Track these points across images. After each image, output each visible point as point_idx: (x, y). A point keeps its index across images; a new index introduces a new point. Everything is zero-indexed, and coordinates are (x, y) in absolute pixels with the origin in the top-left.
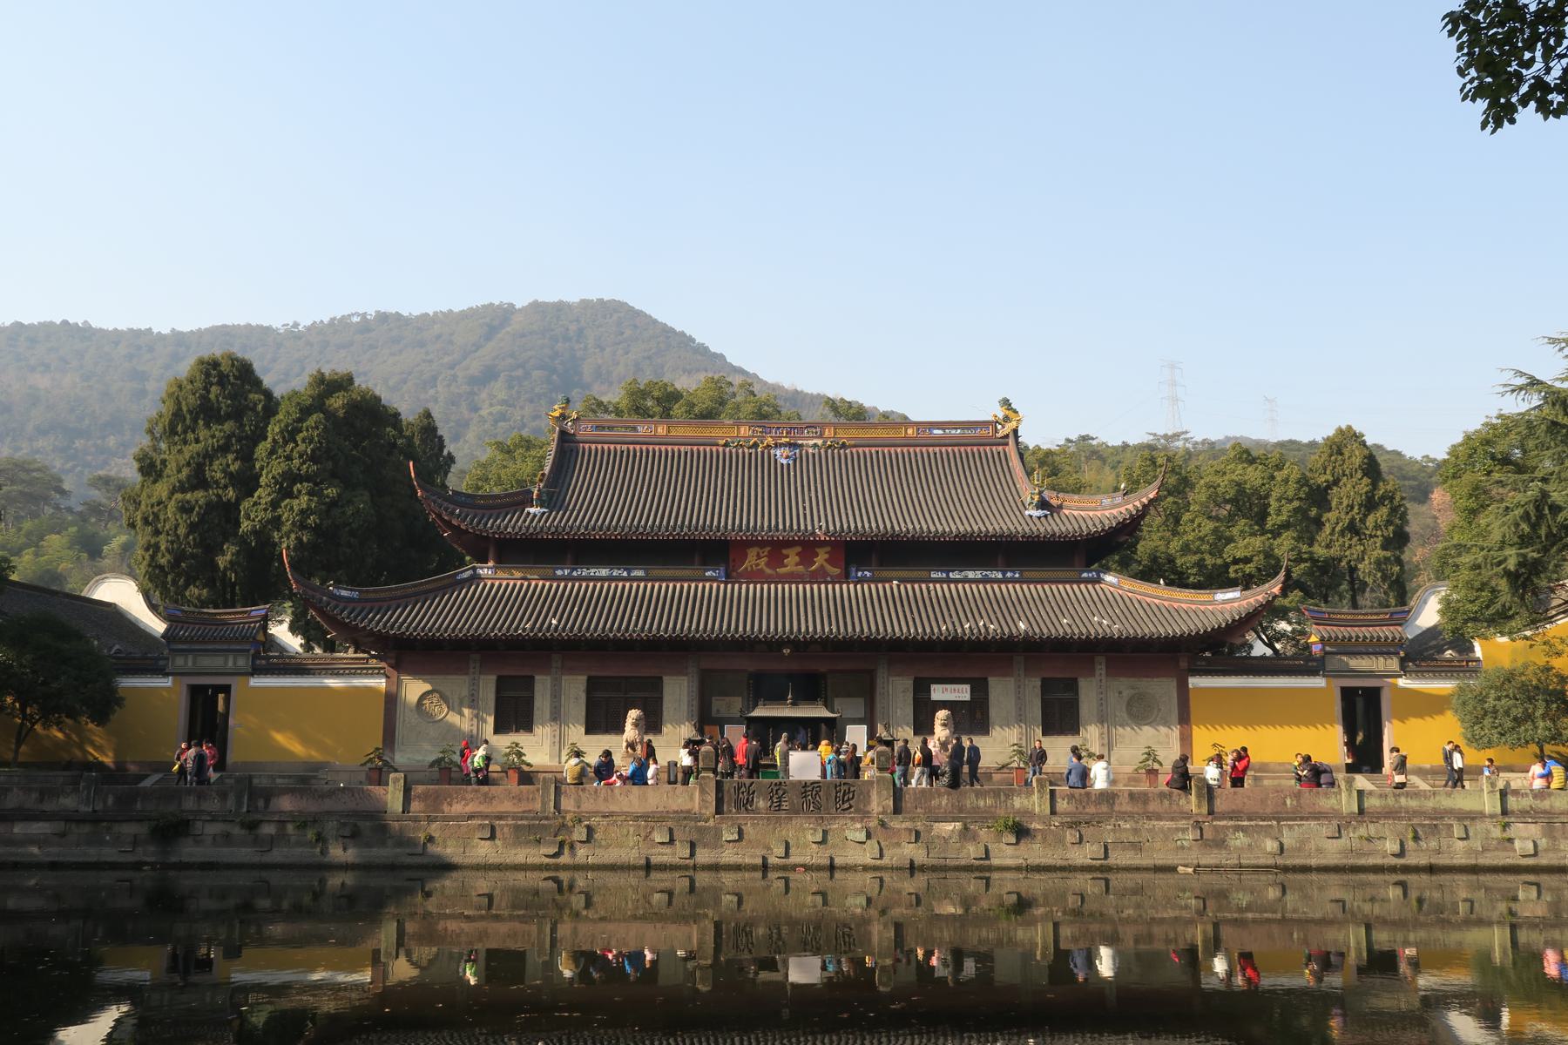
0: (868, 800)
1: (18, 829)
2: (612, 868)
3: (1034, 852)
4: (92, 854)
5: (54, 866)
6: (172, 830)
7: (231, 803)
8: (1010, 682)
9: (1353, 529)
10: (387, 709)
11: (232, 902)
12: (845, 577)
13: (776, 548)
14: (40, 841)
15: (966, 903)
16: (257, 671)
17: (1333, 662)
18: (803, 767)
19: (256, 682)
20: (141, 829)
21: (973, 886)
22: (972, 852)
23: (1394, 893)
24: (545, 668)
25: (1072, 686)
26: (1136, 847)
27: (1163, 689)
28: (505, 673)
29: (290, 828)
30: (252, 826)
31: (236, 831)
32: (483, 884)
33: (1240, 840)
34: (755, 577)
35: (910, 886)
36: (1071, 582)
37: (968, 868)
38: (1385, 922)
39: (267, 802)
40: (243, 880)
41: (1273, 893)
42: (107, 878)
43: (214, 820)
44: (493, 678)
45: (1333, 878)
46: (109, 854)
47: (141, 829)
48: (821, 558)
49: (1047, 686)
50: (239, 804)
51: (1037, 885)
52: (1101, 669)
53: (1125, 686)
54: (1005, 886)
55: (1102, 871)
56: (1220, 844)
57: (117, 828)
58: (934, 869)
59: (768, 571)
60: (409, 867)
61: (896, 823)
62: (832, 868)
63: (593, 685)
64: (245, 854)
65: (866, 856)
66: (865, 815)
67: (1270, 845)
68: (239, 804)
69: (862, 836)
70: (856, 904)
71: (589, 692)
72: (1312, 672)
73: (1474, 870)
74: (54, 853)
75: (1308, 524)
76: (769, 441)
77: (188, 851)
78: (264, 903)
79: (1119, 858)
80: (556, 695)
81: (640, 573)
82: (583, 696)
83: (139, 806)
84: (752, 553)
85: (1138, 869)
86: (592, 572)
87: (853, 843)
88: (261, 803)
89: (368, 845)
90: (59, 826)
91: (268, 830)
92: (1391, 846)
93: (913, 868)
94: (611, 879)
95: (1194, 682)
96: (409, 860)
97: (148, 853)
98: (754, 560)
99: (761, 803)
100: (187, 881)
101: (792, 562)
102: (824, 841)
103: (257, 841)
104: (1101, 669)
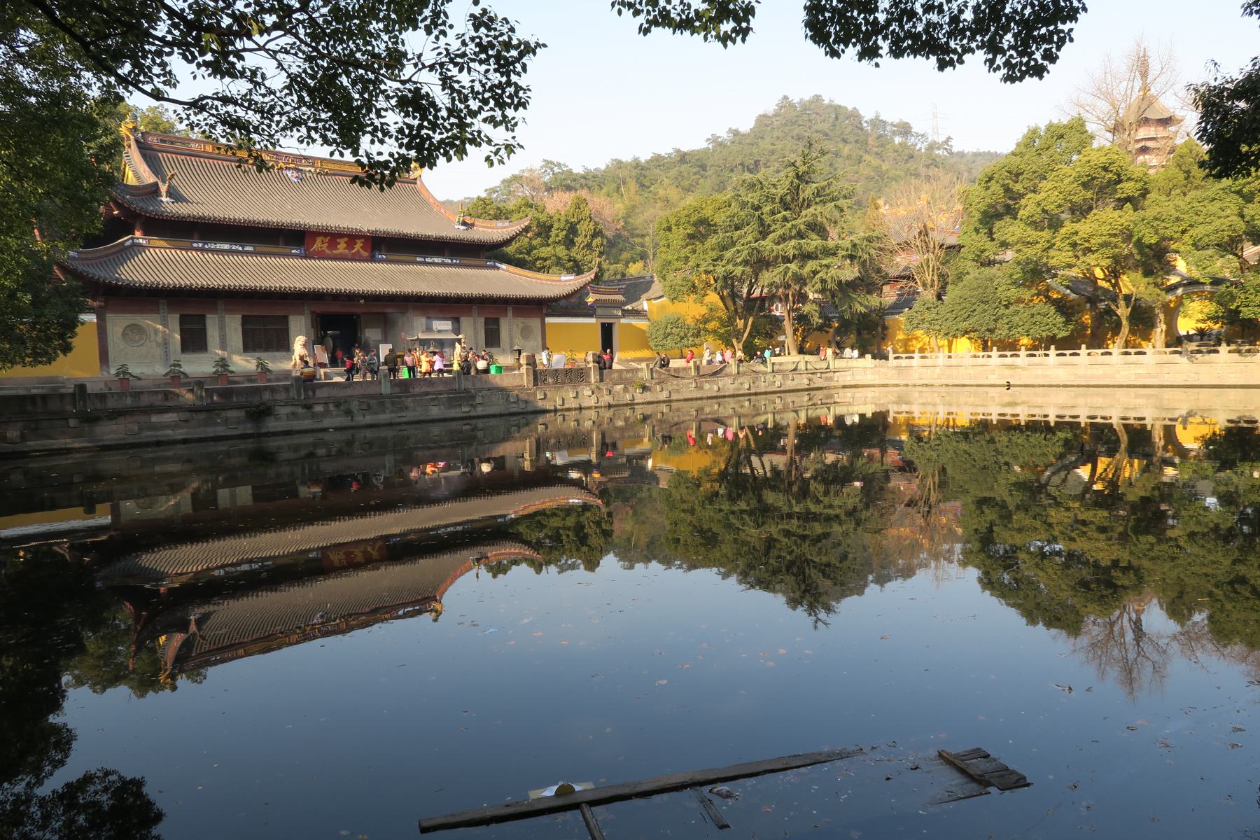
0: (589, 376)
1: (155, 419)
2: (494, 416)
3: (648, 396)
4: (210, 431)
5: (185, 441)
6: (260, 413)
7: (293, 393)
8: (470, 320)
9: (589, 246)
10: (99, 333)
11: (303, 453)
12: (372, 259)
13: (333, 236)
14: (174, 426)
15: (627, 419)
16: (624, 316)
17: (599, 311)
18: (558, 362)
19: (623, 321)
20: (241, 414)
21: (628, 413)
22: (628, 397)
23: (747, 404)
24: (214, 310)
25: (202, 319)
26: (678, 391)
27: (535, 323)
28: (185, 313)
29: (331, 407)
30: (308, 407)
31: (300, 410)
32: (369, 434)
33: (707, 386)
34: (321, 256)
35: (608, 414)
36: (186, 250)
37: (627, 405)
38: (745, 416)
39: (314, 392)
40: (309, 439)
41: (716, 407)
42: (222, 447)
43: (286, 405)
44: (483, 320)
45: (731, 400)
46: (221, 430)
47: (241, 414)
48: (359, 245)
49: (183, 320)
50: (299, 395)
51: (649, 410)
52: (510, 313)
53: (520, 322)
54: (639, 410)
55: (668, 402)
56: (702, 388)
57: (224, 414)
58: (616, 406)
59: (328, 252)
60: (400, 424)
61: (601, 385)
62: (1009, 386)
63: (245, 321)
64: (307, 424)
65: (592, 402)
66: (589, 383)
67: (716, 388)
68: (299, 395)
69: (590, 393)
70: (588, 424)
71: (181, 324)
72: (591, 316)
73: (766, 393)
74: (180, 434)
75: (569, 243)
76: (281, 164)
77: (272, 425)
78: (321, 452)
79: (674, 397)
80: (222, 328)
81: (251, 249)
82: (240, 328)
83: (235, 399)
84: (319, 239)
85: (701, 399)
86: (219, 246)
87: (587, 396)
88: (310, 393)
89: (376, 413)
90: (184, 416)
91: (319, 408)
92: (747, 386)
93: (610, 406)
94: (493, 422)
95: (549, 320)
96: (399, 420)
97: (249, 428)
98: (319, 244)
99: (550, 380)
100: (272, 444)
101: (342, 247)
102: (576, 397)
103: (314, 416)
104: (510, 313)
